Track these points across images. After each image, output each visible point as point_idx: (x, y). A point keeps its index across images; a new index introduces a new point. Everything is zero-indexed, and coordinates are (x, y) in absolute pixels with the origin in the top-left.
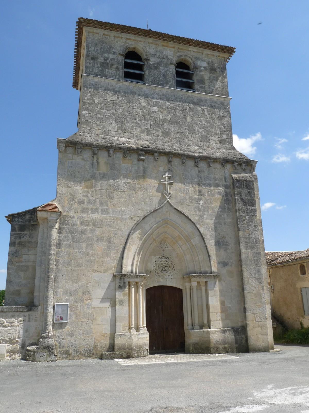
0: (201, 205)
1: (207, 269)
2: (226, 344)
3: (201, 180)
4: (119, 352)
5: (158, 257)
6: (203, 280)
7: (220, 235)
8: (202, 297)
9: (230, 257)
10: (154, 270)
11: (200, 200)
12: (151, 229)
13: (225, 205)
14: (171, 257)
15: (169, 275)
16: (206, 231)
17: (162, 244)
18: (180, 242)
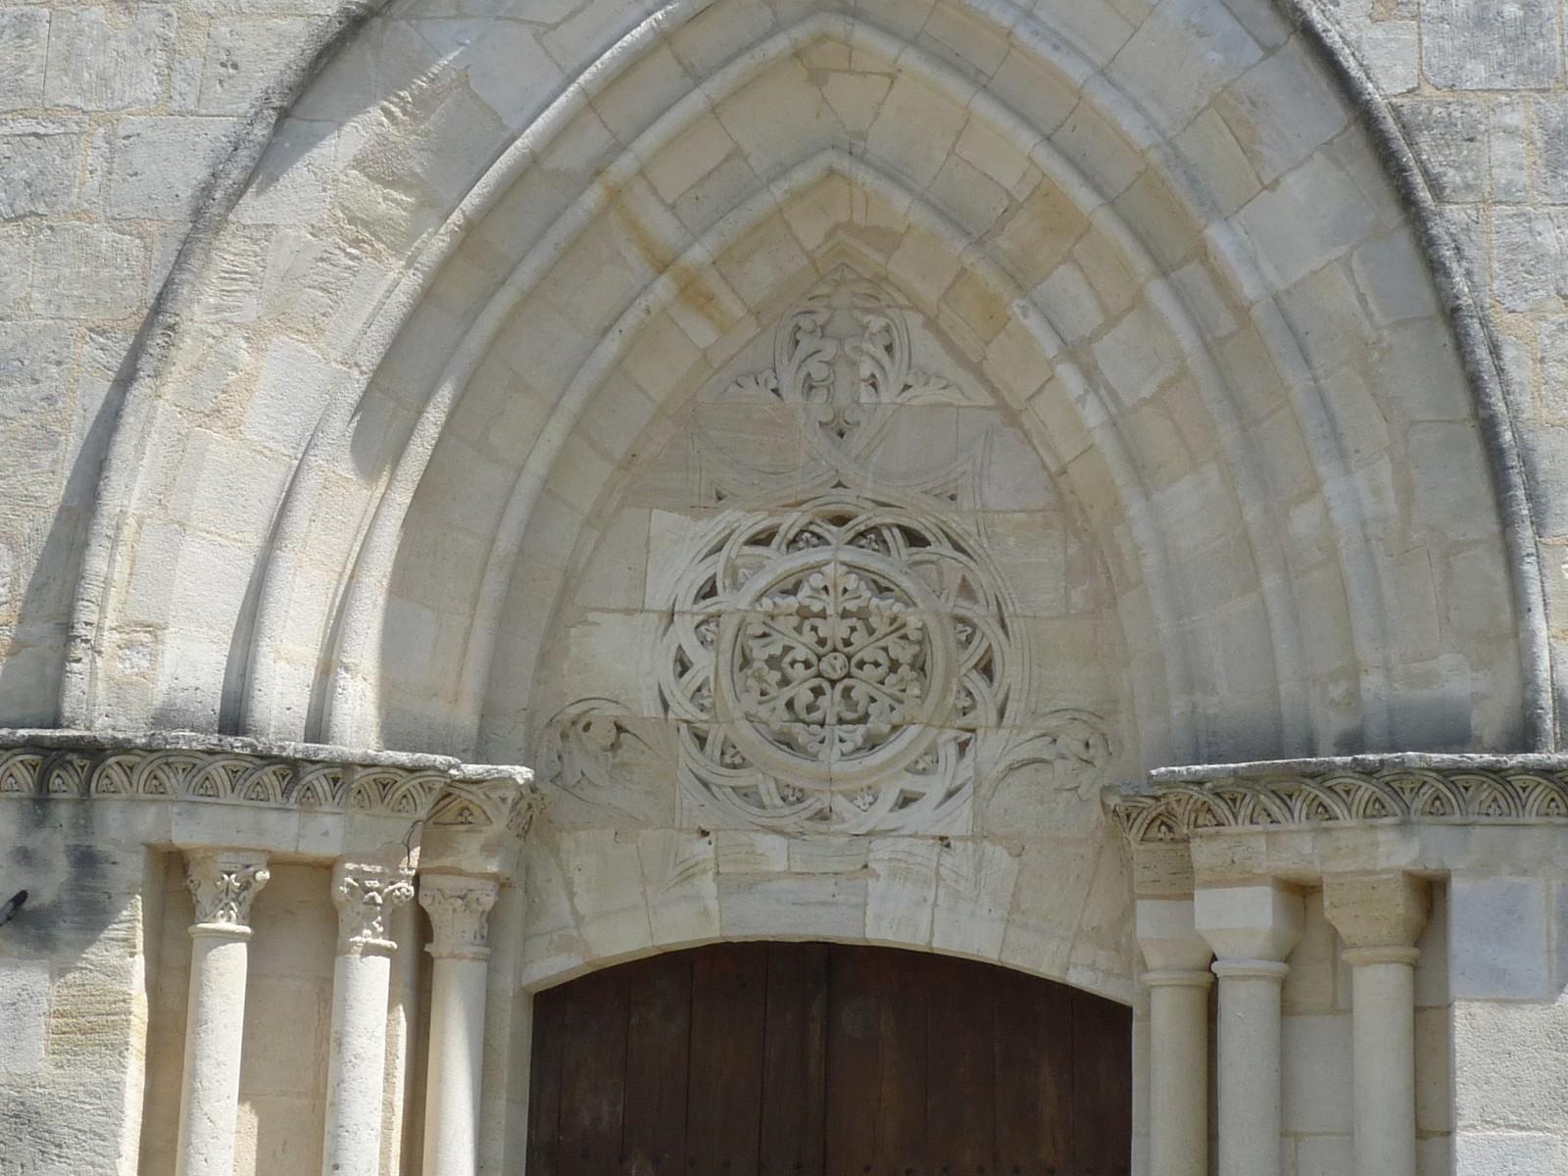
1: (1456, 680)
5: (760, 522)
10: (683, 708)
12: (572, 88)
14: (958, 524)
15: (911, 783)
16: (1477, 72)
17: (823, 331)
18: (1065, 283)
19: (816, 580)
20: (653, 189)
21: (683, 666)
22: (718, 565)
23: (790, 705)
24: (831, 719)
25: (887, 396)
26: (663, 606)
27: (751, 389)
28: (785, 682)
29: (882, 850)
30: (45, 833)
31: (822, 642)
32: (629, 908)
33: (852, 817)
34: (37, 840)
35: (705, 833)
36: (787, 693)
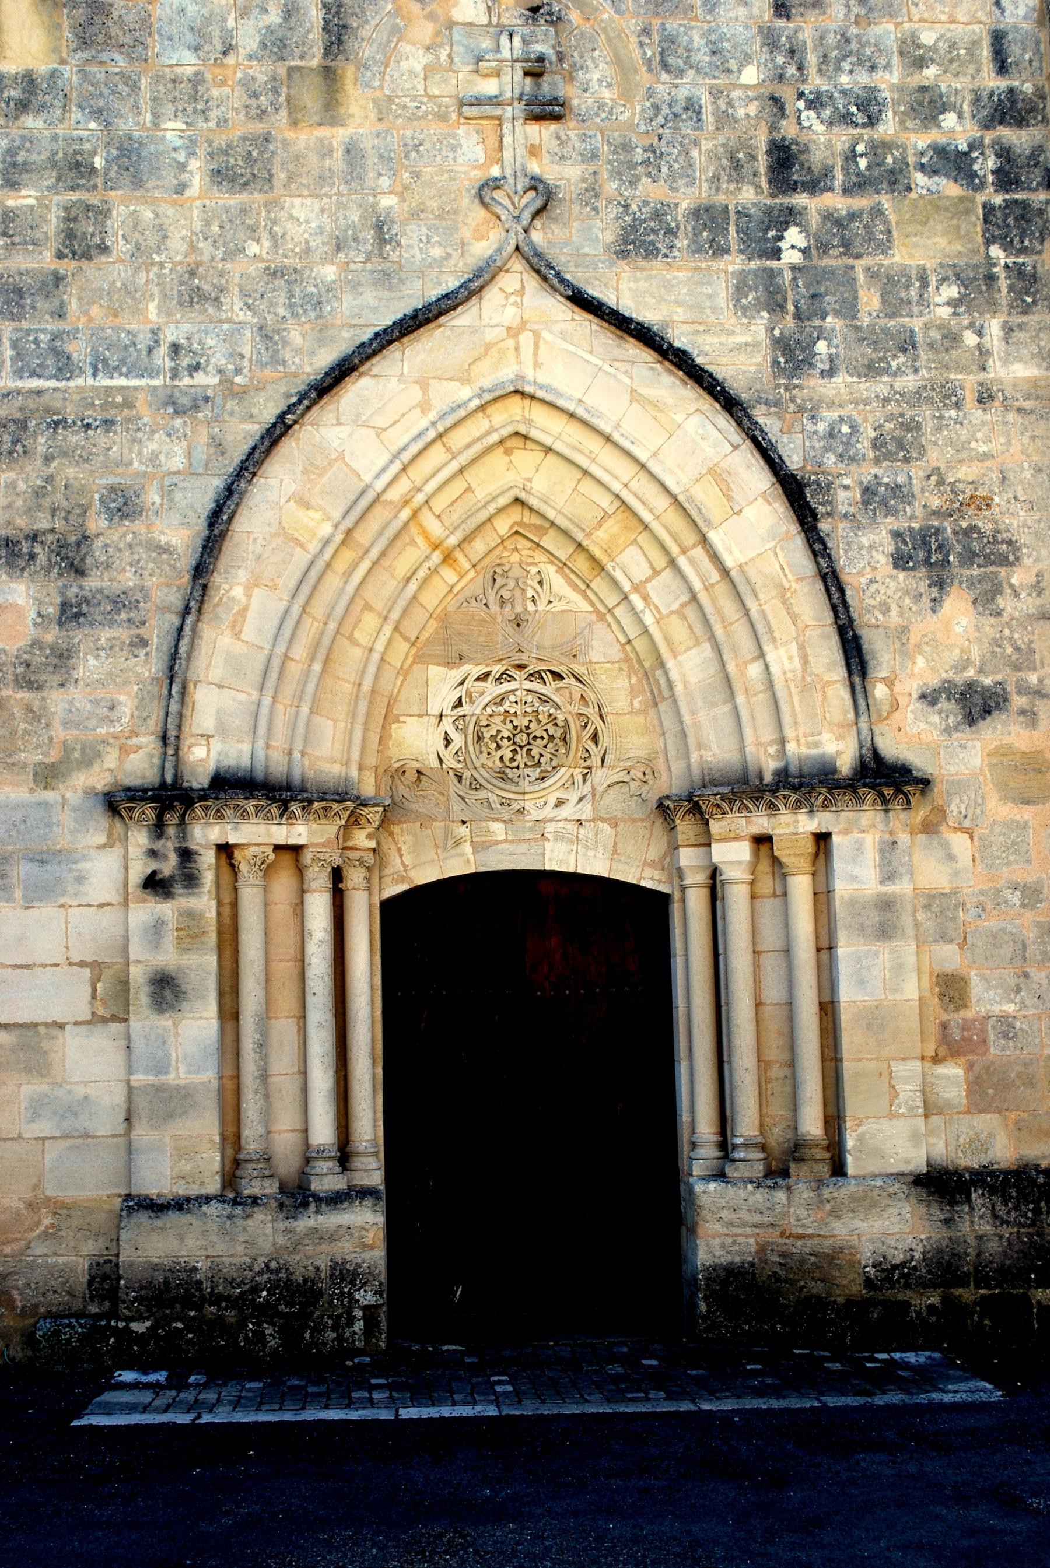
0: (794, 268)
2: (962, 1281)
3: (792, 70)
4: (148, 1324)
5: (482, 669)
6: (794, 826)
7: (941, 482)
8: (787, 951)
9: (1017, 649)
10: (450, 762)
11: (786, 225)
13: (996, 251)
14: (579, 669)
19: (512, 698)
20: (430, 508)
21: (448, 742)
22: (462, 692)
23: (501, 758)
24: (522, 766)
25: (541, 607)
26: (438, 713)
27: (473, 603)
28: (499, 747)
29: (550, 828)
30: (163, 841)
31: (515, 728)
32: (424, 860)
33: (535, 814)
34: (158, 845)
35: (464, 822)
36: (500, 753)
